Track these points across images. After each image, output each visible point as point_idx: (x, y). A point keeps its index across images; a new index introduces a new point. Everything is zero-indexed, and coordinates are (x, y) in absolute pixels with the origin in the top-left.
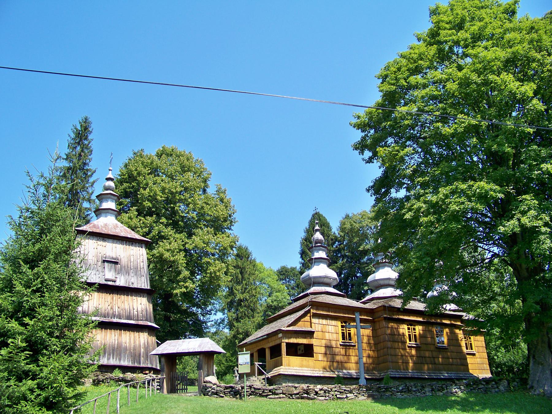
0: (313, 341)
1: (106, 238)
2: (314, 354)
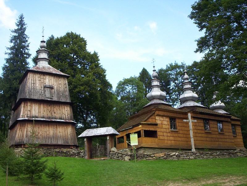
0: (158, 130)
1: (44, 74)
2: (158, 136)
